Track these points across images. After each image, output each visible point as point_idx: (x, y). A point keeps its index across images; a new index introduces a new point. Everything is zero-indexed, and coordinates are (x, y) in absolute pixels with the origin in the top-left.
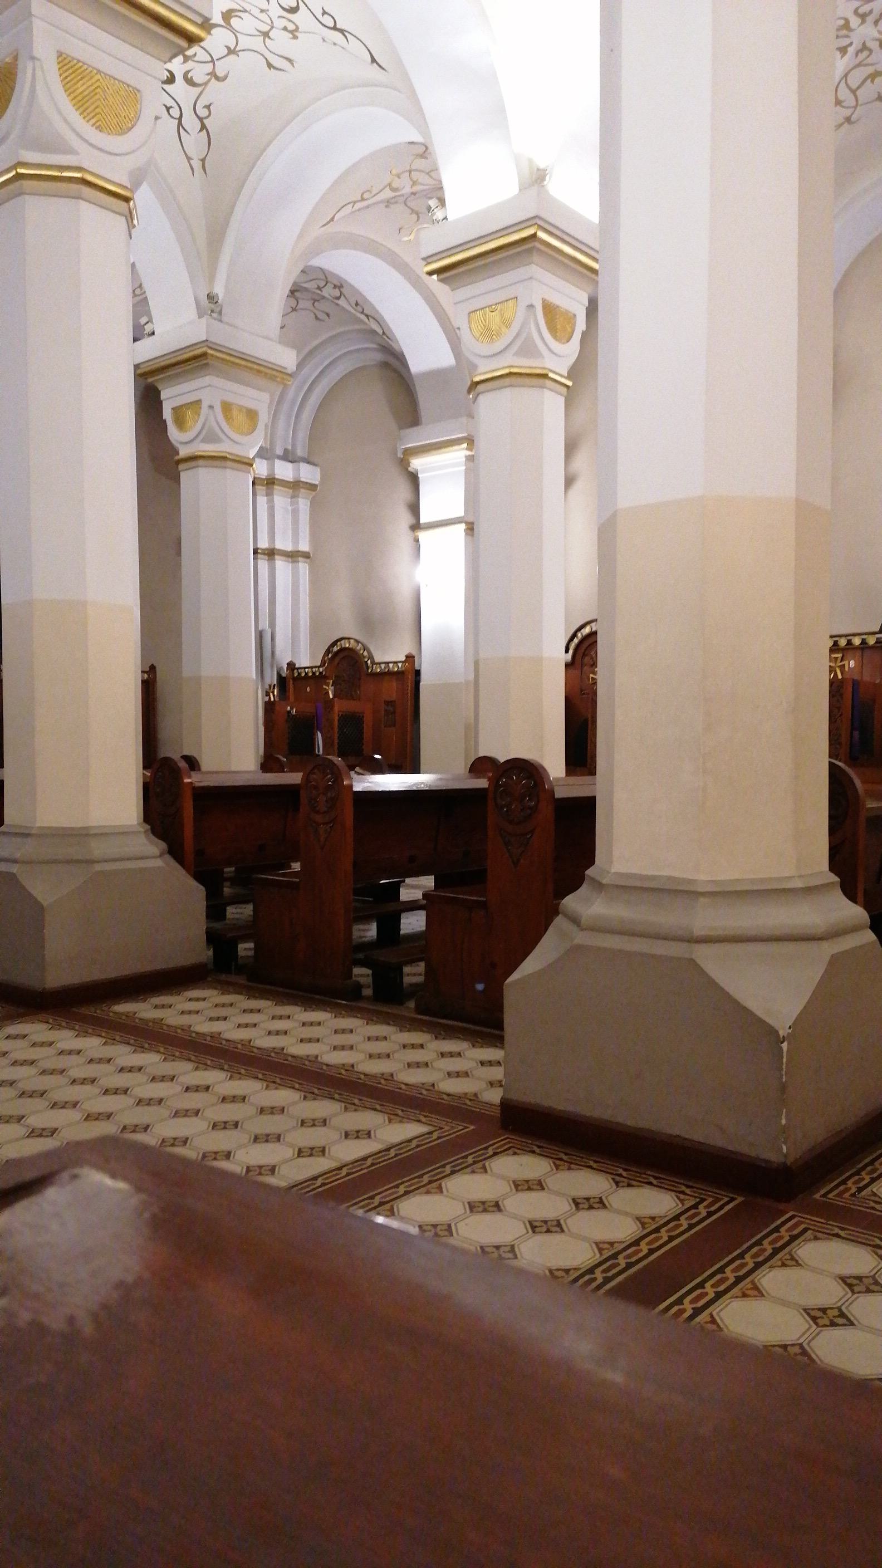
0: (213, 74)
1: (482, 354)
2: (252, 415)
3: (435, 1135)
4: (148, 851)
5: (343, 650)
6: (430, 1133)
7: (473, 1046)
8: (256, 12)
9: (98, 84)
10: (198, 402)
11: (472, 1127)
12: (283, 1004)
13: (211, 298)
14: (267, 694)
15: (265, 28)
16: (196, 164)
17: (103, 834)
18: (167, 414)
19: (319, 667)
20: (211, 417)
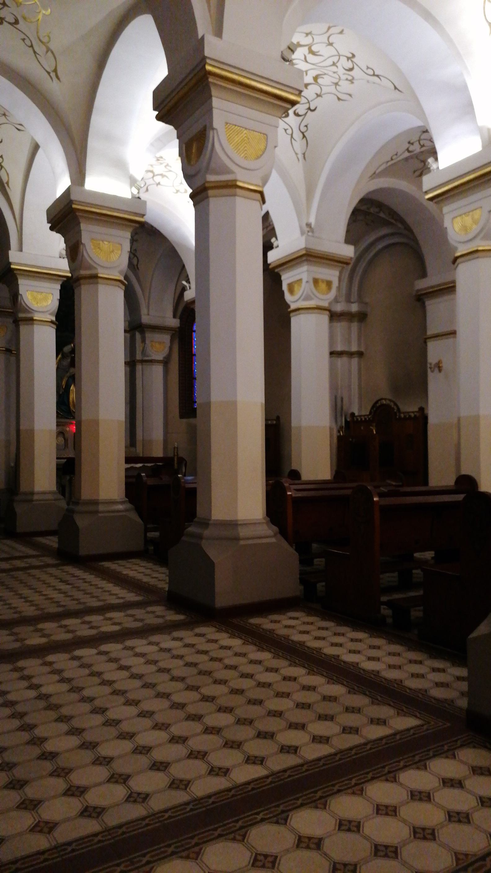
0: (309, 109)
1: (462, 240)
2: (329, 284)
3: (425, 727)
4: (267, 531)
5: (382, 405)
6: (423, 726)
7: (453, 665)
8: (331, 73)
9: (246, 135)
10: (300, 280)
11: (449, 724)
12: (341, 625)
13: (309, 225)
14: (339, 432)
15: (336, 81)
16: (300, 156)
17: (246, 524)
18: (285, 287)
19: (368, 415)
20: (305, 288)
